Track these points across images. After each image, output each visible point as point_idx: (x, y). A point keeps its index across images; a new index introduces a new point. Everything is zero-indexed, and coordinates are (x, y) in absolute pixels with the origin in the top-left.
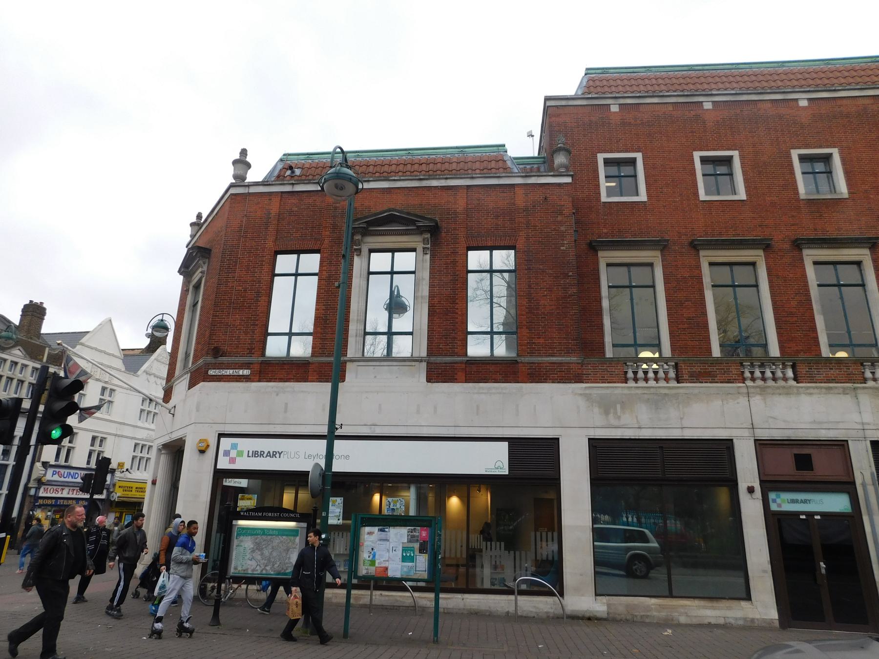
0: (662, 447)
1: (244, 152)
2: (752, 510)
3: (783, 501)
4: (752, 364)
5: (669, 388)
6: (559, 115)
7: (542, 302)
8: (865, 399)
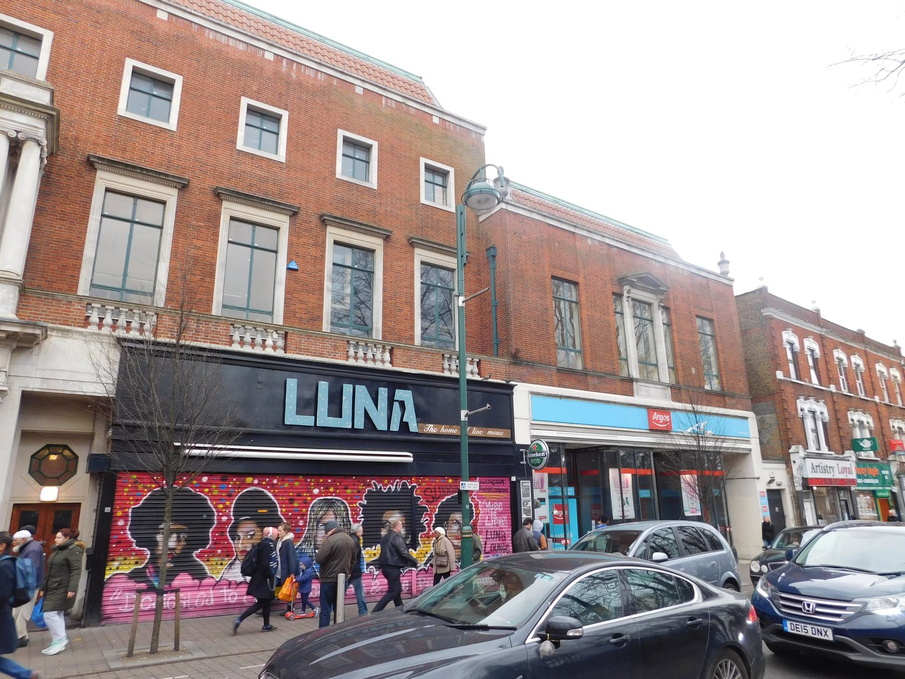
1: (722, 255)
4: (357, 343)
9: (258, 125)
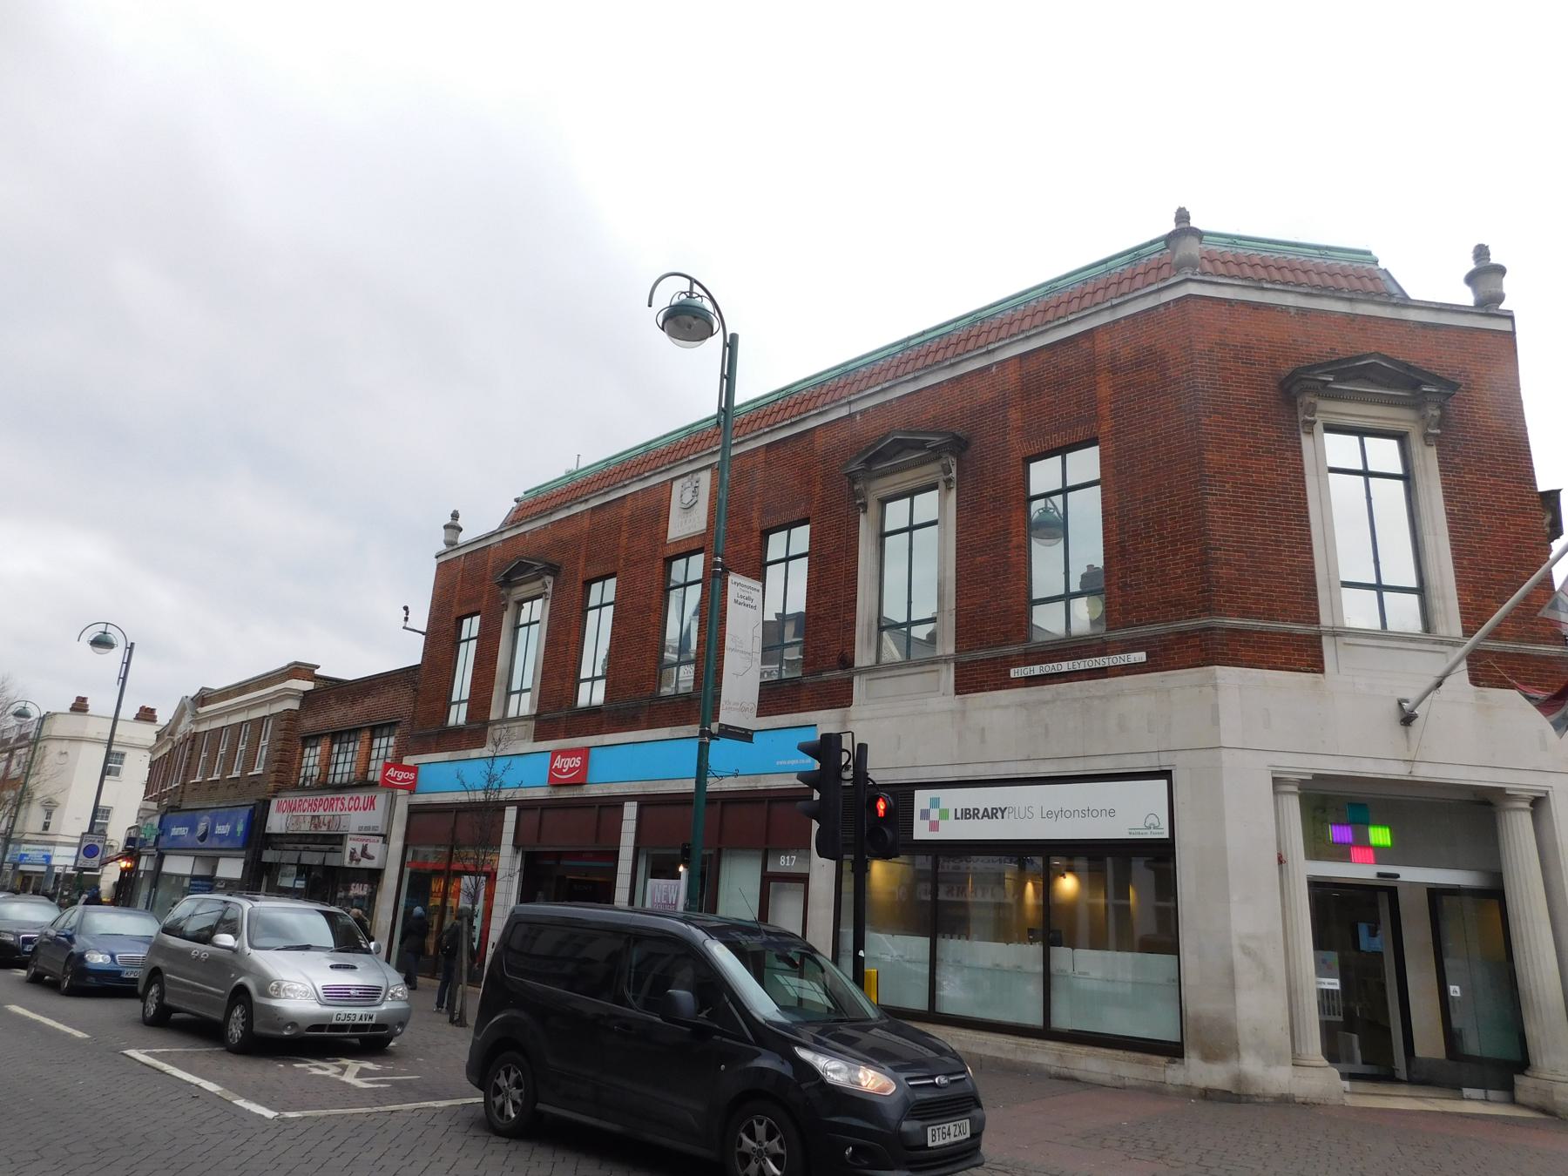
1: (455, 516)
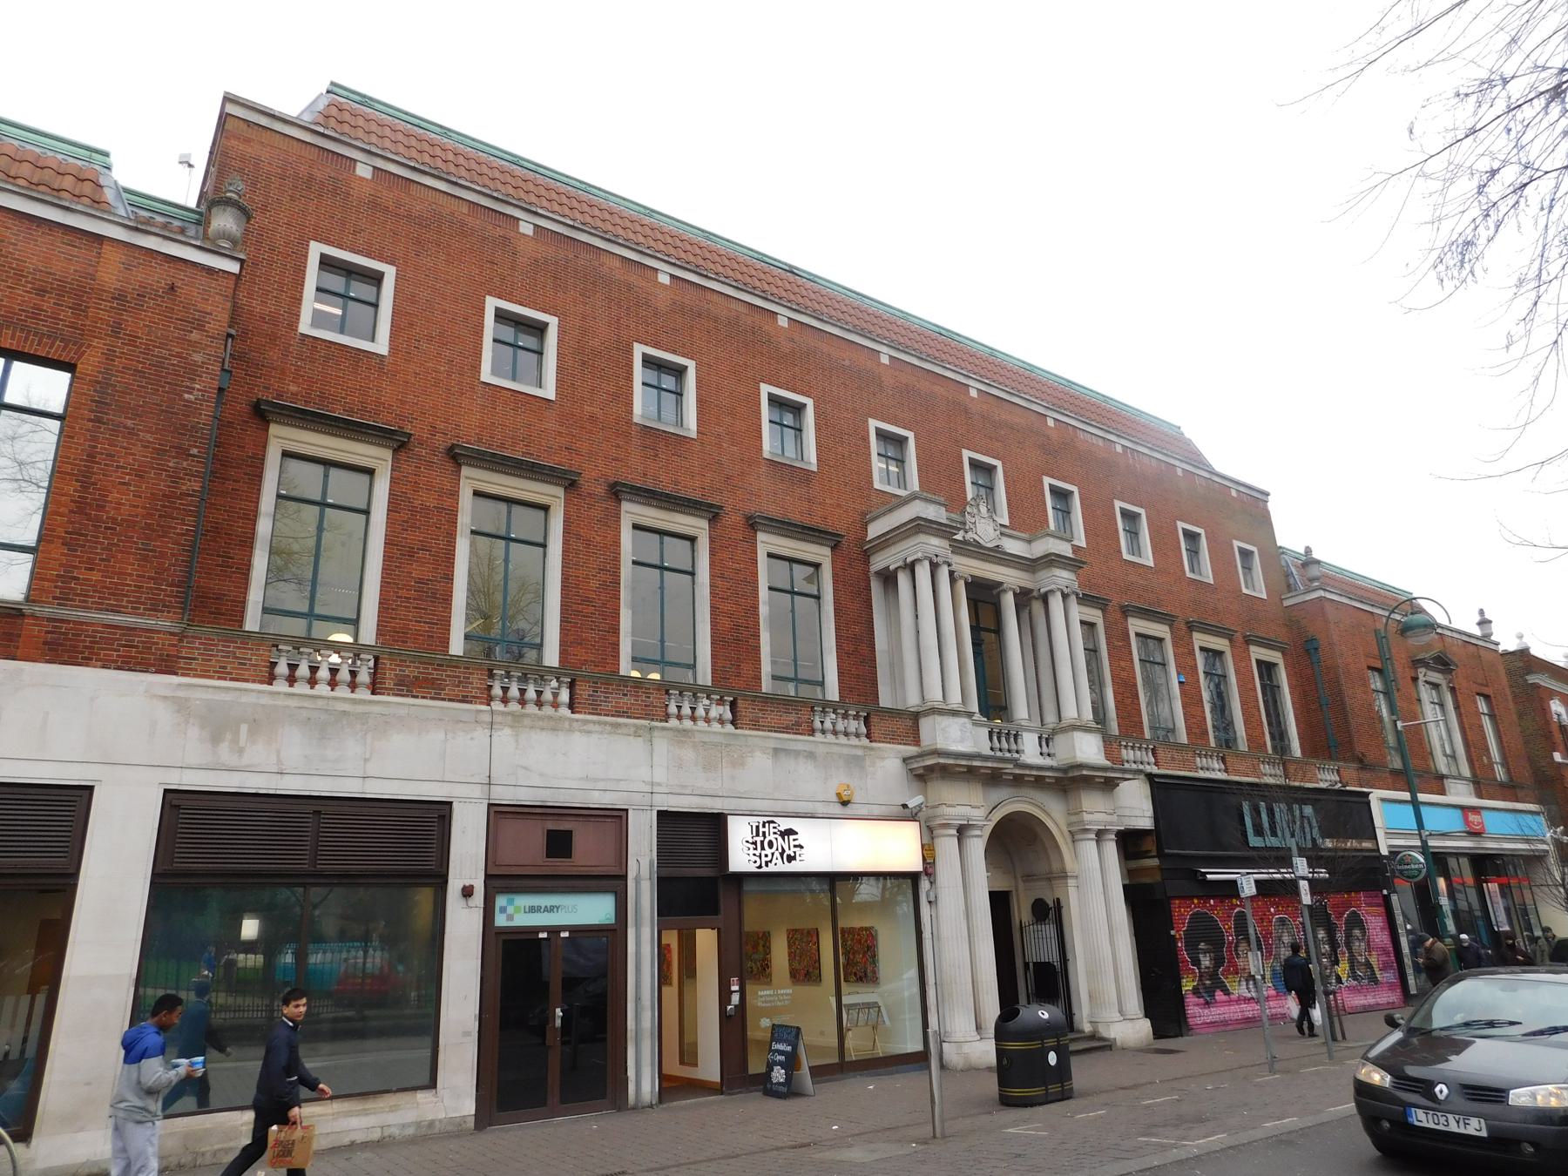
0: (319, 812)
1: (1481, 612)
2: (463, 931)
3: (517, 910)
5: (354, 701)
6: (248, 141)
7: (114, 496)
8: (662, 744)
9: (511, 341)
